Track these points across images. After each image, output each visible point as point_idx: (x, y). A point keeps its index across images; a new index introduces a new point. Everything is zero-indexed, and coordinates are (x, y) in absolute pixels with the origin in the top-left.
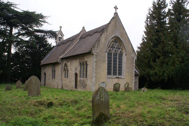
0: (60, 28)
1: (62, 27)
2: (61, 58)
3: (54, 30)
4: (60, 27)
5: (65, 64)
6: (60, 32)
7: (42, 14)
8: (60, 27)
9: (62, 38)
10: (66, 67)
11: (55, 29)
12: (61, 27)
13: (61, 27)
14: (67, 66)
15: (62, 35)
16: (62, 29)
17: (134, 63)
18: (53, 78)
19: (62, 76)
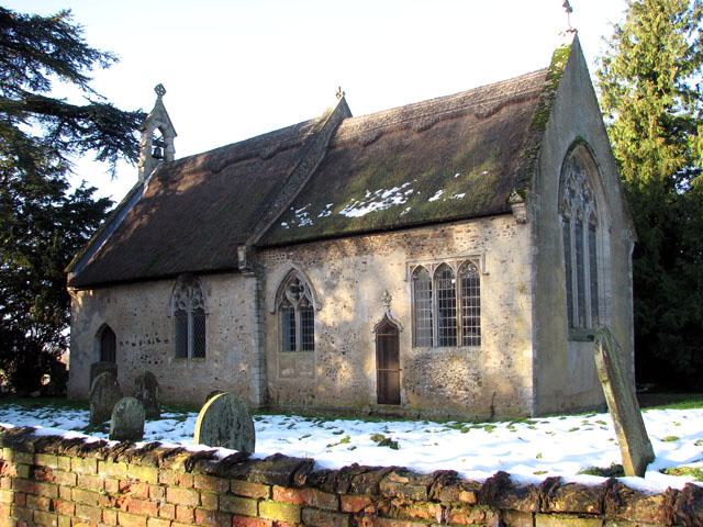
0: (156, 97)
1: (164, 92)
2: (254, 246)
3: (125, 105)
4: (156, 89)
5: (285, 280)
6: (160, 112)
7: (71, 22)
8: (156, 89)
9: (165, 146)
10: (289, 294)
11: (129, 96)
12: (160, 90)
13: (160, 90)
14: (296, 290)
15: (169, 131)
16: (164, 98)
17: (628, 270)
18: (182, 353)
19: (262, 343)
